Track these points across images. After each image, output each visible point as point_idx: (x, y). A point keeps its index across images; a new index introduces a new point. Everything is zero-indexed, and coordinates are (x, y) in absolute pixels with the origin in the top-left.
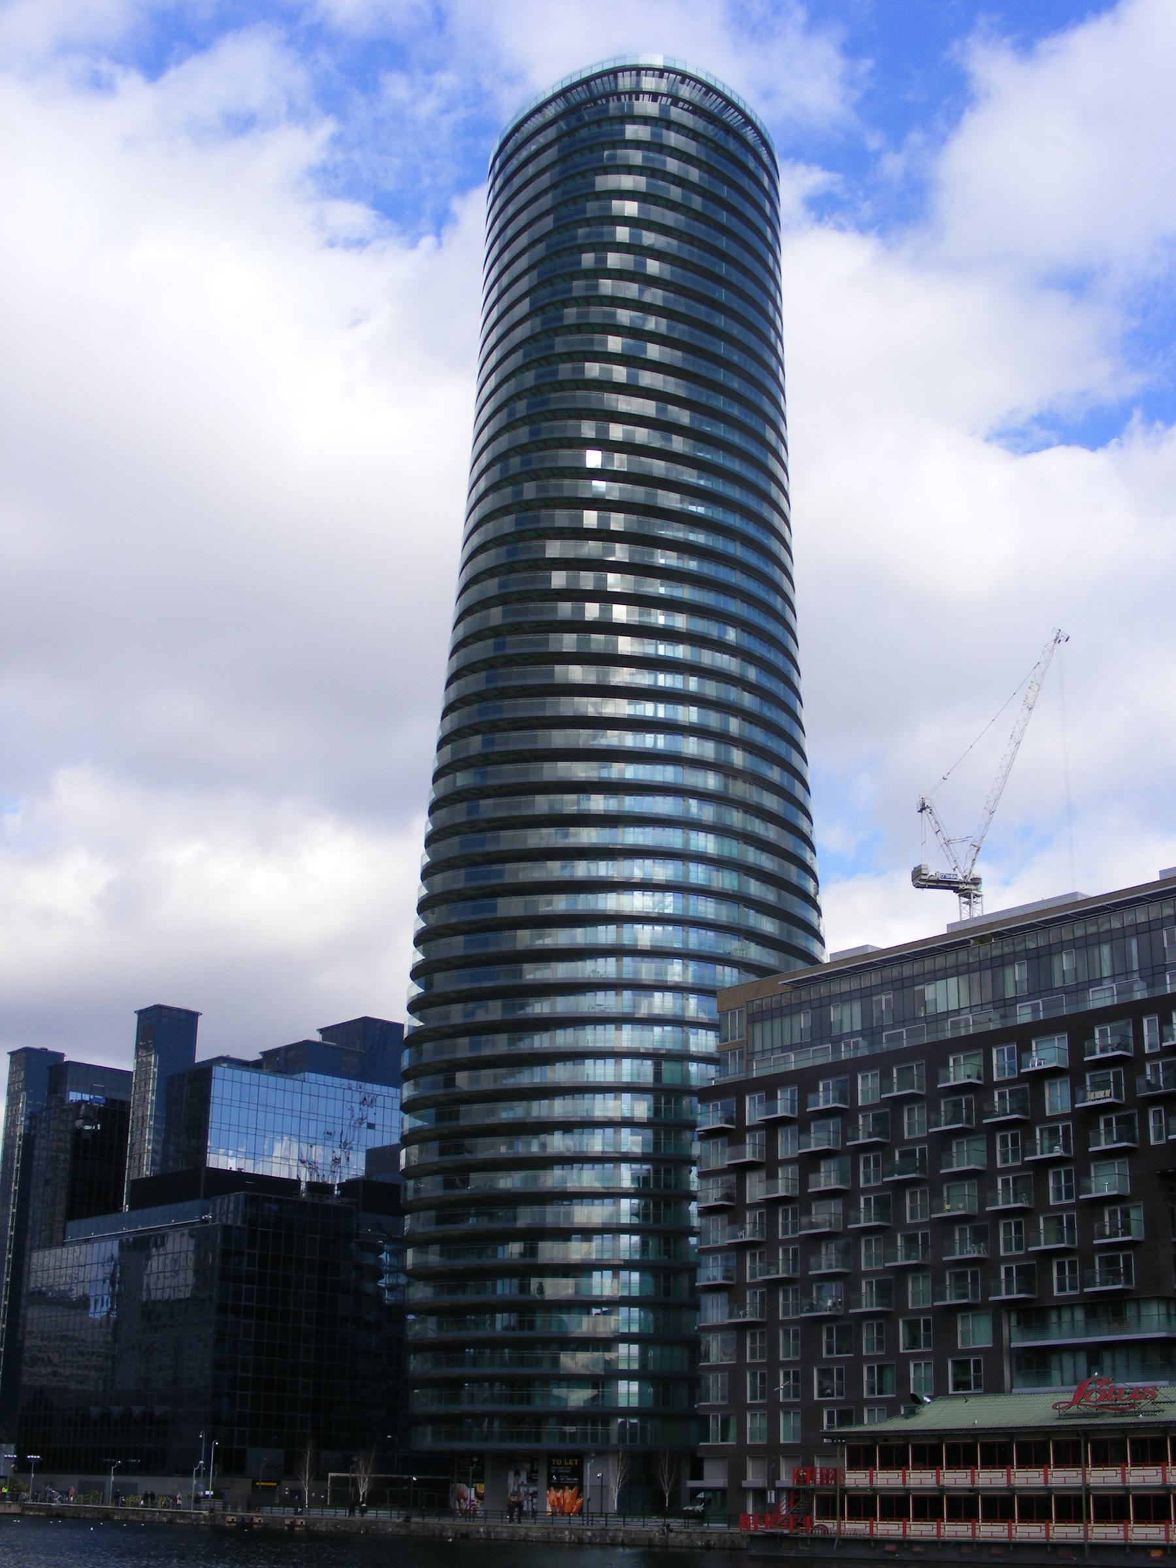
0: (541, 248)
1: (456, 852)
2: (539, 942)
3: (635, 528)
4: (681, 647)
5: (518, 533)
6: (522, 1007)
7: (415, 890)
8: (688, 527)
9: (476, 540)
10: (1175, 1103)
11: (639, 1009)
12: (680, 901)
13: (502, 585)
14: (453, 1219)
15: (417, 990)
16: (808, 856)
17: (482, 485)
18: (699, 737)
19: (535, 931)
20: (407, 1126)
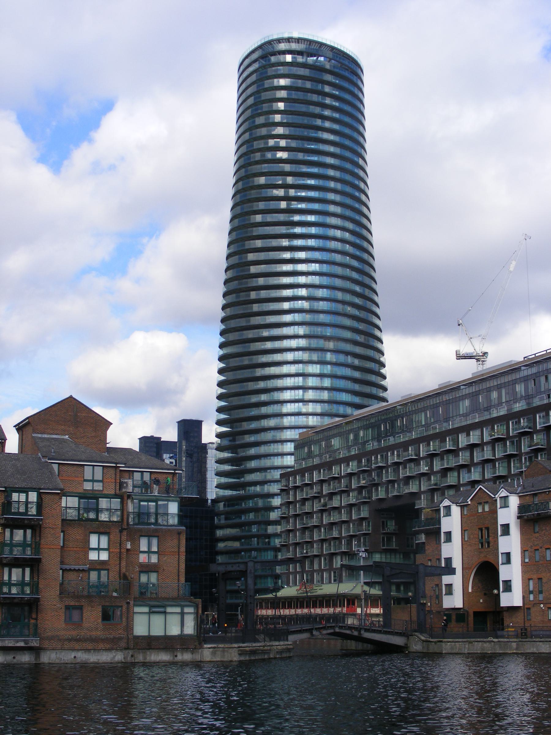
0: (249, 111)
1: (237, 262)
2: (255, 387)
3: (292, 157)
4: (253, 461)
5: (263, 81)
6: (293, 217)
7: (221, 301)
8: (307, 166)
9: (240, 141)
10: (550, 451)
11: (301, 398)
12: (329, 292)
13: (242, 209)
14: (233, 505)
15: (223, 327)
16: (374, 286)
17: (242, 129)
18: (335, 182)
19: (255, 383)
20: (219, 392)
